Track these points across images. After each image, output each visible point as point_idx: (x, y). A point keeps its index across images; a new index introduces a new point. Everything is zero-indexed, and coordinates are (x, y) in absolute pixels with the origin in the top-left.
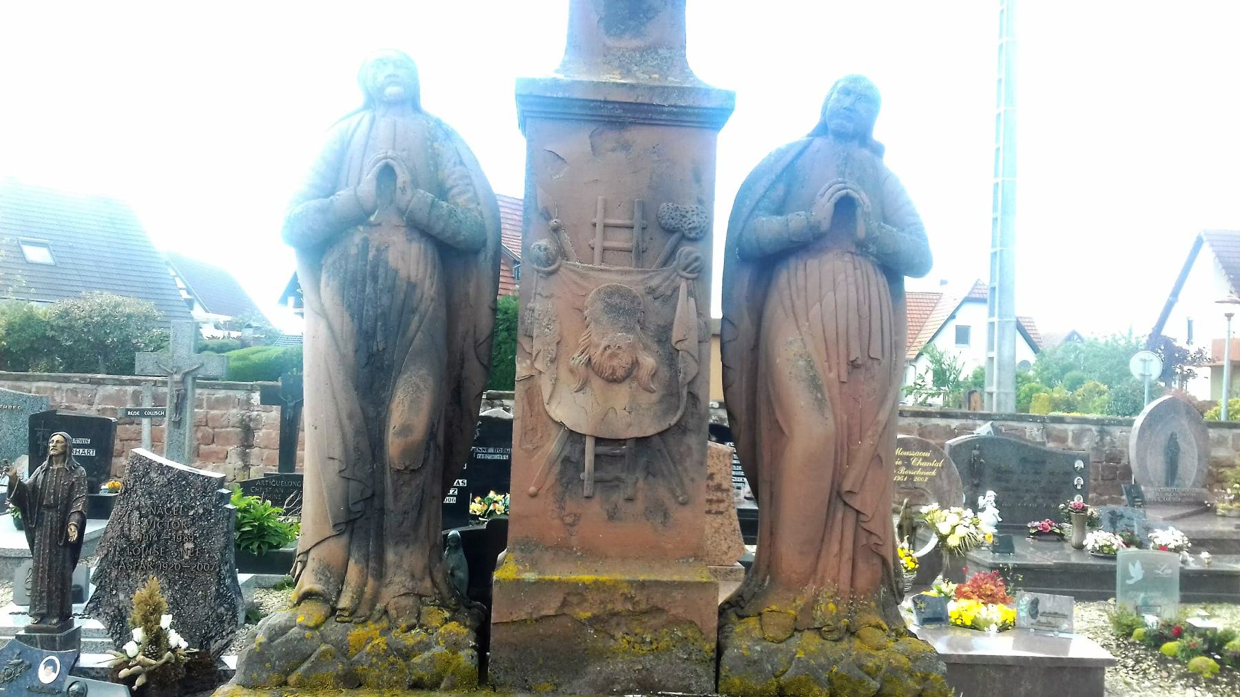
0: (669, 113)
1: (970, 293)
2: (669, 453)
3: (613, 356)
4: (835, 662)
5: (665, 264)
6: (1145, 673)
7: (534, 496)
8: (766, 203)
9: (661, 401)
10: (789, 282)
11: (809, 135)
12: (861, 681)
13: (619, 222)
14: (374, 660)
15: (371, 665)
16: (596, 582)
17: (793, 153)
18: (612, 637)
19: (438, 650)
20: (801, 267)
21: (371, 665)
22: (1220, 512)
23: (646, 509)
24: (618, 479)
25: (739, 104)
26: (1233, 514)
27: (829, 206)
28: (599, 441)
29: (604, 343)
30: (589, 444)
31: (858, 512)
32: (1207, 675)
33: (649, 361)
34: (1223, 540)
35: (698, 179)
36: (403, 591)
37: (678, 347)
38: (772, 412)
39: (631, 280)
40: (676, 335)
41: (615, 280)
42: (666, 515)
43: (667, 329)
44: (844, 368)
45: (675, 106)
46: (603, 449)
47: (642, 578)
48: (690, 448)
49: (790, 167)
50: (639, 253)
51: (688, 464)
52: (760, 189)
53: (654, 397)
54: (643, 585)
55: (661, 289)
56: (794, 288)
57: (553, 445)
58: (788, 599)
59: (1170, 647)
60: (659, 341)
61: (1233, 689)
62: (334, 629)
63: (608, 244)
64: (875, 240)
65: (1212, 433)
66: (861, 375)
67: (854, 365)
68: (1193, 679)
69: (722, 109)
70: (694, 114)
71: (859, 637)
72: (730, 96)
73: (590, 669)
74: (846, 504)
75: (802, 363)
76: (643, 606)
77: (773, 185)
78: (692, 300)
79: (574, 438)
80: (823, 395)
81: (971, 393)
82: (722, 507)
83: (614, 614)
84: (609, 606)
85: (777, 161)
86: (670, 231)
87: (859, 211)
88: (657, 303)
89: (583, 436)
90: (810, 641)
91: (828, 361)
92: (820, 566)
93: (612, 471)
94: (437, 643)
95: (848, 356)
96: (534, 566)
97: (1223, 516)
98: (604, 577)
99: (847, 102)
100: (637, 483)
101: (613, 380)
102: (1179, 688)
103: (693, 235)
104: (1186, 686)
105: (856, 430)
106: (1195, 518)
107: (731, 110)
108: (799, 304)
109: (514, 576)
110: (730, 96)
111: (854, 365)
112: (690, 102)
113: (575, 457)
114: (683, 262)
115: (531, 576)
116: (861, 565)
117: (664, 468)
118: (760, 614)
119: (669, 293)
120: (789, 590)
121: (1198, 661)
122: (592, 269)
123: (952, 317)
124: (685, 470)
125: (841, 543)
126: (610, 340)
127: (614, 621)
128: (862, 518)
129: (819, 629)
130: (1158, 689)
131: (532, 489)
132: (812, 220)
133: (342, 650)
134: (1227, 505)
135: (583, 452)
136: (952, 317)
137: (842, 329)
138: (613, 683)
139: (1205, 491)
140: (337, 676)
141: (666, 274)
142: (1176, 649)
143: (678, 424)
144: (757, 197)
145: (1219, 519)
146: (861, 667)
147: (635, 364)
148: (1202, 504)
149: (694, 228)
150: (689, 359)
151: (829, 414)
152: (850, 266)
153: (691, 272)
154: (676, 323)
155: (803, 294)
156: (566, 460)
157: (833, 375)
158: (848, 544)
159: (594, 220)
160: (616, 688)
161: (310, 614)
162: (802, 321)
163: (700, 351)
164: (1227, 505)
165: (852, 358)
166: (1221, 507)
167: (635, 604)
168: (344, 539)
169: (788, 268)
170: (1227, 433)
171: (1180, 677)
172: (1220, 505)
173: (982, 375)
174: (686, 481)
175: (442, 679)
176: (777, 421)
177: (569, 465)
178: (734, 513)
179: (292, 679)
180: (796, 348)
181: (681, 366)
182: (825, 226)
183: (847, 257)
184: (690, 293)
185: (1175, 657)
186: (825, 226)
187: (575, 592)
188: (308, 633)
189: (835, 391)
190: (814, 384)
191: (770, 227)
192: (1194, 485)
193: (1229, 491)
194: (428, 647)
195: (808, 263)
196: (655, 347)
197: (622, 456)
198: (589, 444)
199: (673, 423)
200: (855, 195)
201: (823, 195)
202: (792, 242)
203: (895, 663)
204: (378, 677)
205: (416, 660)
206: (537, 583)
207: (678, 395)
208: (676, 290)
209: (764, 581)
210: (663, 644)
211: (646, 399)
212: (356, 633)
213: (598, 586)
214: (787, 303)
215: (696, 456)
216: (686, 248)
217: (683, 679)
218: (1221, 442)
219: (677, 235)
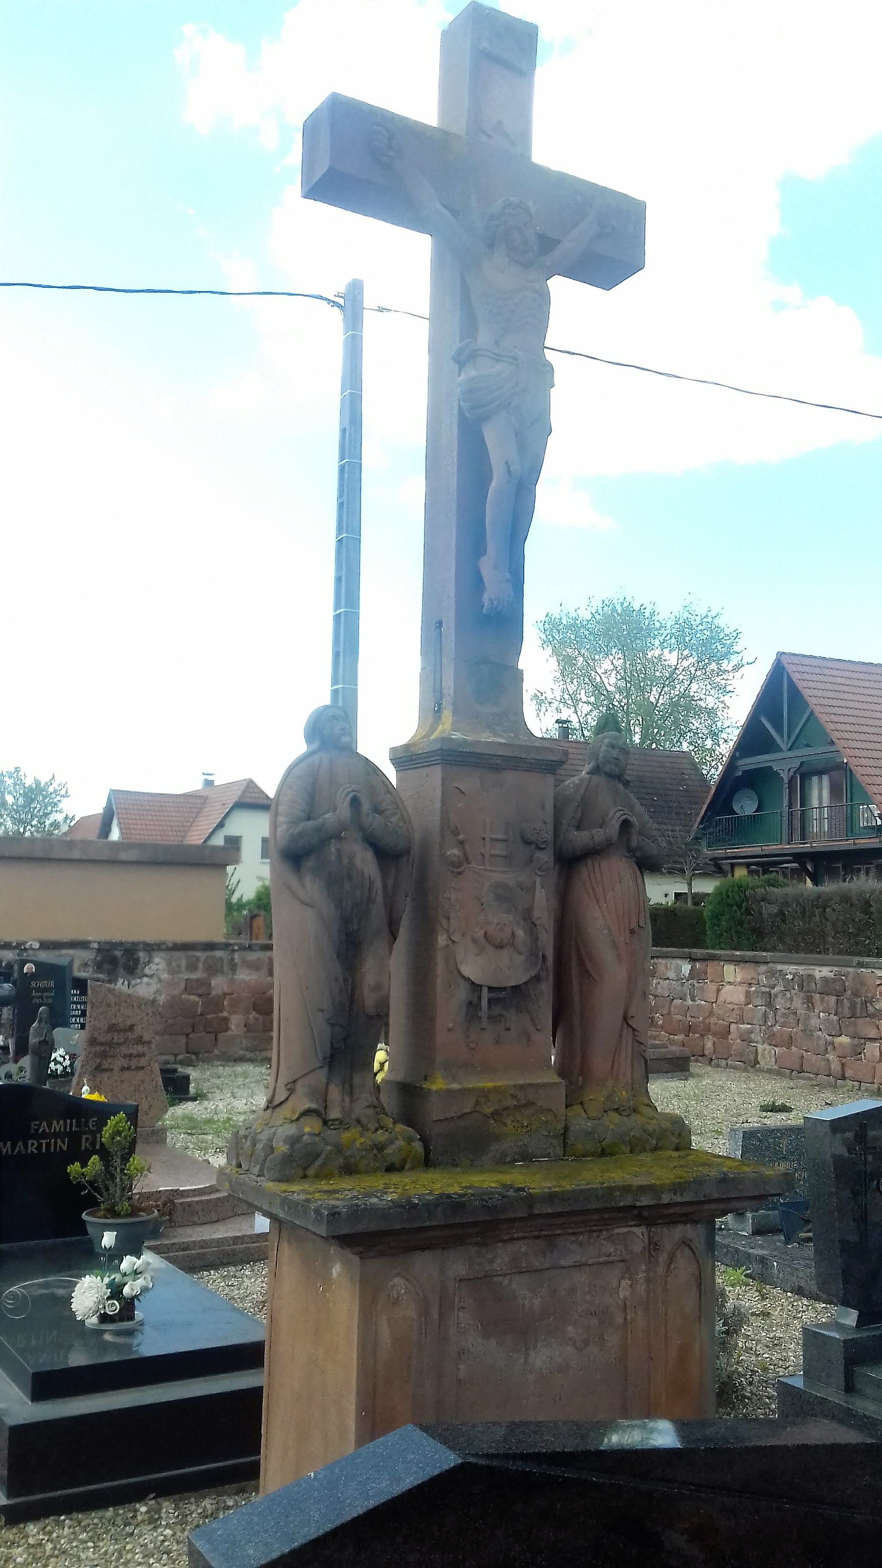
1: (242, 796)
3: (502, 930)
4: (631, 1130)
7: (450, 1030)
12: (647, 1140)
13: (499, 837)
14: (364, 1153)
15: (362, 1157)
16: (495, 1087)
18: (505, 1124)
19: (400, 1143)
20: (597, 865)
21: (362, 1157)
24: (501, 1015)
27: (617, 826)
28: (490, 989)
29: (496, 921)
30: (485, 990)
33: (520, 933)
36: (367, 1104)
38: (582, 964)
39: (509, 878)
40: (536, 913)
41: (497, 877)
46: (493, 995)
47: (521, 1082)
50: (508, 858)
54: (522, 1087)
56: (593, 881)
57: (462, 994)
62: (329, 1133)
63: (493, 852)
71: (638, 1112)
73: (492, 1148)
75: (606, 932)
76: (523, 1102)
79: (476, 987)
81: (253, 917)
82: (143, 1062)
83: (506, 1109)
84: (504, 1103)
89: (481, 986)
90: (615, 1117)
92: (615, 1068)
93: (497, 1010)
94: (397, 1139)
96: (455, 1079)
98: (499, 1084)
99: (615, 753)
100: (512, 1017)
101: (501, 947)
108: (599, 891)
109: (446, 1087)
111: (632, 932)
113: (475, 1001)
115: (455, 1086)
118: (582, 1103)
122: (486, 870)
123: (221, 825)
126: (499, 919)
127: (505, 1113)
129: (617, 1109)
131: (450, 1025)
133: (339, 1149)
135: (480, 997)
136: (221, 825)
138: (506, 1156)
140: (340, 1167)
146: (645, 1131)
147: (513, 935)
156: (470, 1003)
158: (630, 1054)
159: (483, 835)
160: (508, 1159)
161: (310, 1126)
167: (518, 1100)
168: (325, 1070)
173: (268, 896)
175: (405, 1163)
177: (472, 1006)
178: (156, 1067)
179: (311, 1172)
183: (624, 860)
187: (484, 1094)
188: (316, 1139)
190: (615, 946)
194: (392, 1142)
197: (504, 999)
198: (485, 990)
200: (630, 818)
203: (664, 1126)
204: (367, 1165)
205: (388, 1151)
206: (460, 1091)
208: (534, 883)
210: (534, 1127)
211: (520, 959)
212: (346, 1136)
213: (496, 1090)
217: (546, 1149)
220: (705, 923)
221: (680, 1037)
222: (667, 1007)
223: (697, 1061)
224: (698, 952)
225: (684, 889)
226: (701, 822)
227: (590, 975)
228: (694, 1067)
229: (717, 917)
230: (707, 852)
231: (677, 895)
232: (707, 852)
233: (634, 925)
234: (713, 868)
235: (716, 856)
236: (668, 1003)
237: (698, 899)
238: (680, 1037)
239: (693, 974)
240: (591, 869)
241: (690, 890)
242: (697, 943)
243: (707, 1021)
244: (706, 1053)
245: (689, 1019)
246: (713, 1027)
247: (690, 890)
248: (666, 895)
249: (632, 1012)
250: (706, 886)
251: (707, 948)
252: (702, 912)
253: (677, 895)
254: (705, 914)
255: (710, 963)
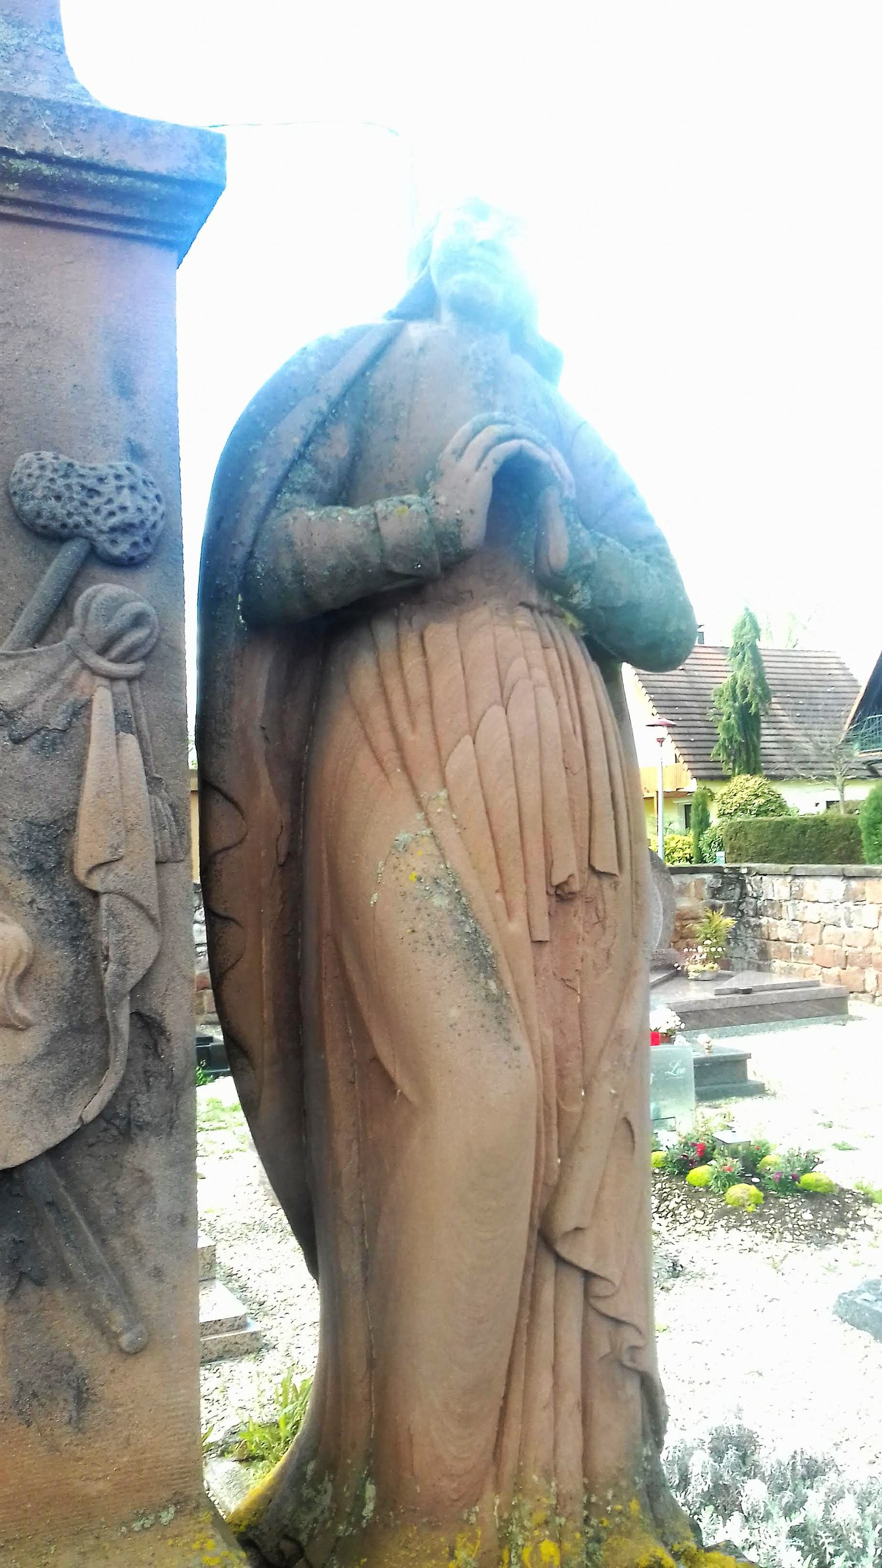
0: (30, 180)
2: (83, 1204)
5: (40, 634)
6: (674, 1215)
8: (306, 473)
9: (49, 1053)
10: (383, 686)
11: (393, 316)
17: (365, 349)
20: (411, 642)
22: (692, 975)
23: (21, 1386)
25: (236, 170)
26: (707, 976)
31: (588, 1276)
32: (750, 1209)
34: (704, 1011)
35: (125, 387)
37: (95, 883)
38: (361, 1034)
40: (88, 847)
42: (82, 1397)
43: (60, 829)
44: (542, 902)
45: (46, 158)
48: (144, 1180)
49: (357, 385)
51: (141, 1228)
52: (291, 435)
53: (30, 1043)
55: (36, 710)
56: (397, 698)
58: (434, 1555)
59: (699, 1174)
60: (37, 871)
61: (784, 1223)
64: (587, 573)
65: (676, 880)
66: (578, 918)
67: (561, 895)
68: (733, 1216)
69: (185, 183)
70: (99, 192)
72: (212, 146)
74: (560, 1260)
75: (440, 901)
77: (321, 429)
78: (131, 742)
80: (500, 982)
85: (325, 367)
86: (49, 536)
87: (552, 498)
88: (24, 754)
91: (502, 890)
92: (511, 1443)
95: (549, 875)
97: (696, 980)
102: (721, 1231)
103: (122, 547)
104: (728, 1229)
105: (573, 1062)
106: (666, 985)
107: (215, 189)
108: (418, 741)
110: (212, 146)
111: (561, 895)
112: (91, 152)
114: (98, 629)
116: (602, 1410)
117: (70, 1257)
119: (58, 721)
120: (434, 1526)
121: (738, 1191)
124: (137, 1250)
125: (555, 1369)
128: (599, 1288)
130: (695, 1236)
132: (442, 515)
134: (699, 967)
137: (532, 803)
139: (673, 951)
141: (47, 665)
142: (707, 1176)
143: (106, 1115)
144: (289, 454)
145: (692, 984)
148: (671, 967)
149: (126, 528)
150: (131, 915)
151: (519, 1037)
152: (533, 640)
153: (123, 658)
154: (85, 812)
155: (423, 714)
157: (516, 927)
162: (430, 788)
163: (162, 896)
164: (699, 967)
165: (557, 879)
166: (692, 969)
169: (375, 648)
170: (689, 879)
171: (719, 1216)
172: (691, 968)
174: (140, 1281)
176: (376, 1059)
180: (420, 861)
181: (108, 938)
182: (474, 531)
183: (524, 618)
184: (124, 722)
185: (707, 1187)
186: (474, 531)
189: (526, 967)
190: (482, 961)
191: (323, 534)
192: (660, 945)
193: (700, 948)
195: (428, 635)
196: (24, 888)
199: (91, 1112)
200: (541, 455)
201: (459, 453)
202: (391, 575)
207: (103, 1028)
208: (81, 710)
209: (360, 1500)
214: (384, 741)
215: (164, 1202)
216: (104, 590)
218: (683, 891)
219: (72, 551)
220: (860, 833)
221: (835, 971)
222: (818, 934)
223: (856, 998)
224: (853, 869)
225: (835, 795)
226: (851, 724)
227: (390, 1083)
228: (854, 1006)
229: (873, 825)
230: (858, 754)
231: (829, 804)
232: (858, 754)
233: (567, 866)
234: (868, 773)
235: (870, 758)
236: (819, 930)
237: (851, 808)
238: (835, 971)
239: (848, 896)
240: (388, 659)
241: (842, 797)
242: (852, 857)
243: (868, 950)
244: (868, 988)
245: (845, 948)
246: (874, 958)
247: (842, 797)
248: (817, 804)
249: (569, 1216)
250: (860, 793)
251: (864, 862)
252: (856, 821)
253: (829, 804)
254: (859, 823)
255: (868, 882)
